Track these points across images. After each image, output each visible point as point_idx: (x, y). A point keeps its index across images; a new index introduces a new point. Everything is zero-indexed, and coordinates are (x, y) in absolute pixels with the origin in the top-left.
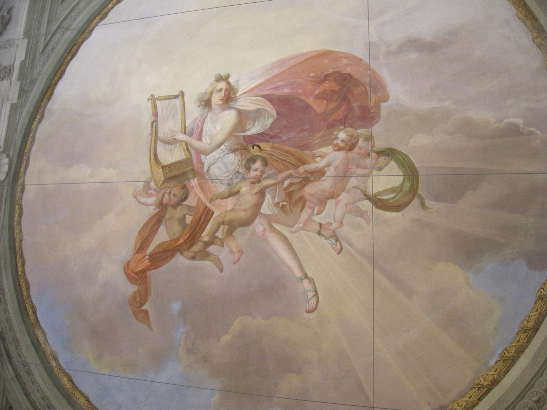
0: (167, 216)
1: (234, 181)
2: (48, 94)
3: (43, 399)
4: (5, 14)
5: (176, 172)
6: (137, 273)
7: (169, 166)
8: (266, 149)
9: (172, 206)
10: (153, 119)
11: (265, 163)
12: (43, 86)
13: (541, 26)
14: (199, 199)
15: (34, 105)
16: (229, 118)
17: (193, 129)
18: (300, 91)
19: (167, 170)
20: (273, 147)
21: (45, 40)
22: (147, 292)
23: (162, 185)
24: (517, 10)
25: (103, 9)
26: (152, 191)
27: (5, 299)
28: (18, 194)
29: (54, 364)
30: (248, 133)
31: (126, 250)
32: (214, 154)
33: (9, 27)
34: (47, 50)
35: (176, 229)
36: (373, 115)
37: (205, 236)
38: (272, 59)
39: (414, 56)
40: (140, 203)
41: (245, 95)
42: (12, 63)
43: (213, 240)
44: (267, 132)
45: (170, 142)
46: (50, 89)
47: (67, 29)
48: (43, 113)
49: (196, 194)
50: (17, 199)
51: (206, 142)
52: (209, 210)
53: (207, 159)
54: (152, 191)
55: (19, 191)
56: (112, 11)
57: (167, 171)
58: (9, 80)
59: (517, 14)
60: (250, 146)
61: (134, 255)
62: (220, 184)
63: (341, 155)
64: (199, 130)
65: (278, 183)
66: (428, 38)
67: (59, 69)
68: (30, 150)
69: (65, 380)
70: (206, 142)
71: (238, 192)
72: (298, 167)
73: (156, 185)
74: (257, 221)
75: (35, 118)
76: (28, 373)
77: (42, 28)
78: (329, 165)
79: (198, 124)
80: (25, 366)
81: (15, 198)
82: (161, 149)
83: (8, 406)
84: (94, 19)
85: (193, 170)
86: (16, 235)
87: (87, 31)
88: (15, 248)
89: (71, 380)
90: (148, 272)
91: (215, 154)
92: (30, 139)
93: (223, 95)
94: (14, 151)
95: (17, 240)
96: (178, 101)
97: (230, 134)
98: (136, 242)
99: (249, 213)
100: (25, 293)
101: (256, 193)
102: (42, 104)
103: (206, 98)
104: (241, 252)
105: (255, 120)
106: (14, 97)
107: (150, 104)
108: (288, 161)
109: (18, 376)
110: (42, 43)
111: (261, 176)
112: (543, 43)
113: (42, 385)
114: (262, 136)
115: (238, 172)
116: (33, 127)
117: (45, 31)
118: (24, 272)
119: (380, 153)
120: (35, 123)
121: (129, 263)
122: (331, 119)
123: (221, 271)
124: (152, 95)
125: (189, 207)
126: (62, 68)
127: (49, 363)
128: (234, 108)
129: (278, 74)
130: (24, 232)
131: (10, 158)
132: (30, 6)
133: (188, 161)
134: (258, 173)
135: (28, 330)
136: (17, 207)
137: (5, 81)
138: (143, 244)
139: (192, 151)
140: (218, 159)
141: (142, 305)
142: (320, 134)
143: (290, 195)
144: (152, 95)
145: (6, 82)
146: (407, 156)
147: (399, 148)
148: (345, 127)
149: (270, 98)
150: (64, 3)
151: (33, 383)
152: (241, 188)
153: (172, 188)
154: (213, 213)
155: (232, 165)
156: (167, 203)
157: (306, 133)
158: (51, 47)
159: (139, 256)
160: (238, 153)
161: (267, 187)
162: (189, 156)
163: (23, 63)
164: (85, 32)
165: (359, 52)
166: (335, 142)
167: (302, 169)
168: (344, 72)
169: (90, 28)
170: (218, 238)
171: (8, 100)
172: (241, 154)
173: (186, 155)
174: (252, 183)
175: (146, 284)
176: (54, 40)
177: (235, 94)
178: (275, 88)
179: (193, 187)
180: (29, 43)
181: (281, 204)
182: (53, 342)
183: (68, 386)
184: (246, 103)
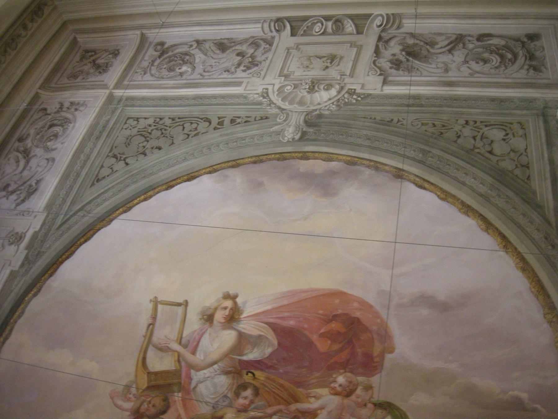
2: (52, 270)
4: (34, 184)
5: (161, 382)
7: (156, 373)
10: (150, 321)
11: (257, 392)
12: (48, 261)
13: (553, 303)
16: (228, 338)
18: (306, 326)
19: (153, 377)
20: (267, 378)
23: (144, 390)
24: (531, 284)
25: (128, 203)
26: (131, 396)
30: (245, 358)
32: (205, 371)
33: (32, 196)
34: (62, 228)
36: (375, 364)
38: (284, 288)
39: (424, 312)
40: (116, 405)
41: (250, 318)
42: (24, 231)
44: (265, 361)
45: (163, 349)
46: (55, 266)
51: (199, 357)
53: (196, 375)
54: (131, 396)
56: (137, 206)
58: (16, 247)
59: (530, 288)
60: (244, 372)
63: (336, 400)
64: (195, 344)
66: (441, 297)
68: (16, 322)
70: (199, 357)
72: (289, 404)
75: (31, 290)
78: (322, 408)
79: (195, 338)
82: (151, 354)
84: (117, 210)
85: (180, 383)
87: (107, 219)
91: (206, 373)
92: (19, 310)
93: (227, 314)
96: (180, 310)
97: (226, 355)
102: (43, 278)
103: (209, 312)
106: (16, 264)
107: (151, 306)
108: (281, 395)
110: (60, 220)
111: (249, 405)
112: (554, 320)
114: (258, 364)
116: (26, 299)
119: (378, 405)
120: (30, 295)
122: (332, 361)
126: (73, 249)
128: (235, 329)
132: (59, 183)
133: (176, 373)
134: (247, 402)
137: (13, 246)
139: (183, 364)
140: (208, 377)
142: (318, 374)
144: (156, 297)
145: (13, 248)
146: (405, 414)
147: (398, 404)
148: (345, 372)
149: (273, 327)
150: (93, 187)
152: (225, 414)
153: (153, 397)
157: (304, 370)
158: (68, 226)
160: (231, 376)
162: (179, 368)
163: (35, 235)
164: (106, 219)
165: (371, 298)
166: (332, 385)
167: (293, 407)
168: (353, 316)
169: (111, 217)
171: (10, 265)
172: (233, 377)
174: (239, 411)
176: (74, 220)
177: (239, 315)
180: (47, 216)
184: (248, 327)
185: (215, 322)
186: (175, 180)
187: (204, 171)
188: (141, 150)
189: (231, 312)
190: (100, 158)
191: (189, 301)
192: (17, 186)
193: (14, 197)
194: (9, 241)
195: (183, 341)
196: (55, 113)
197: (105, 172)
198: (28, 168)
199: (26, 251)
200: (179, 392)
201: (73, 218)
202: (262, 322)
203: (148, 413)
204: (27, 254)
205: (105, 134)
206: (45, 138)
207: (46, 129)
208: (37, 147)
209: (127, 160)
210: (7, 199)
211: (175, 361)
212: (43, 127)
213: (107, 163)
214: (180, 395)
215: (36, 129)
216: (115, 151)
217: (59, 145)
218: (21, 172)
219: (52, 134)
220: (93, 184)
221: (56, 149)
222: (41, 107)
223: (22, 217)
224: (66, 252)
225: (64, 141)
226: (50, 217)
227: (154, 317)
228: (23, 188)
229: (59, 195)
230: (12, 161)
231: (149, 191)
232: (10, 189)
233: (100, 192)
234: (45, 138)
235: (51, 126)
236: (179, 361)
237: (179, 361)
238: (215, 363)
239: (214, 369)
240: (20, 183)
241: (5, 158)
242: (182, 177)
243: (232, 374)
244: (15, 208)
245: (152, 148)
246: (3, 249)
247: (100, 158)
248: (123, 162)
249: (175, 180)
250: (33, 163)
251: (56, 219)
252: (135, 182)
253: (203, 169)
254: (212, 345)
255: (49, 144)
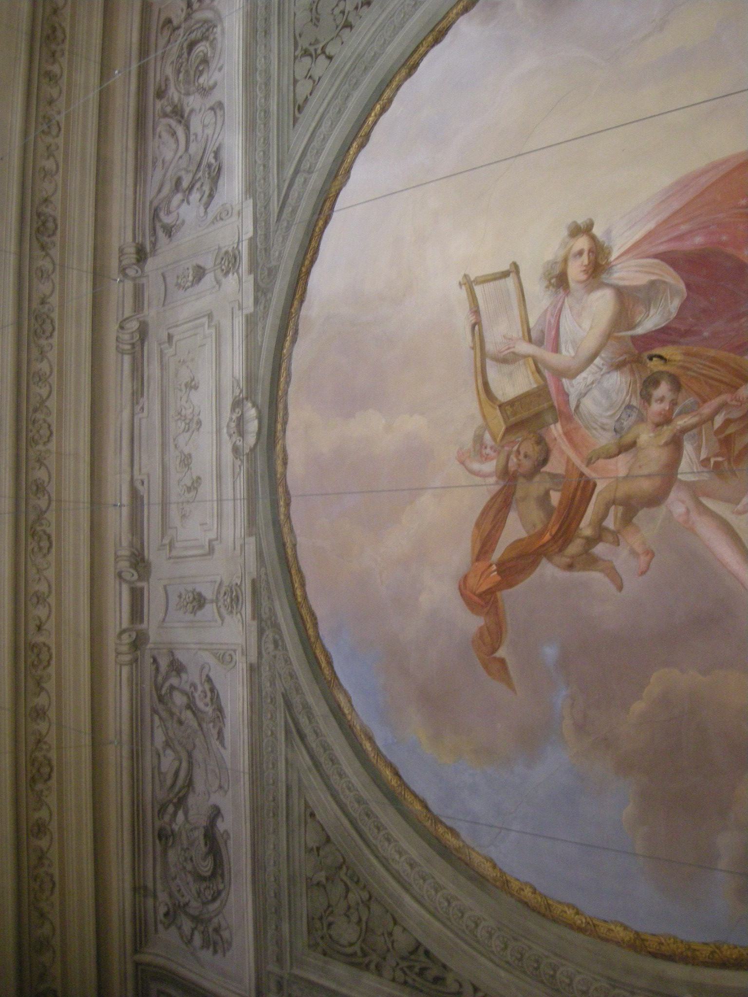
0: (519, 493)
1: (625, 423)
2: (299, 293)
3: (359, 802)
5: (525, 414)
6: (480, 596)
7: (512, 403)
8: (673, 357)
9: (524, 476)
10: (473, 319)
11: (676, 384)
12: (288, 278)
14: (568, 460)
15: (280, 313)
16: (600, 305)
17: (543, 332)
20: (687, 354)
21: (279, 195)
22: (501, 628)
23: (504, 435)
27: (283, 641)
28: (279, 469)
29: (368, 746)
30: (639, 331)
31: (458, 555)
33: (220, 182)
35: (536, 516)
37: (586, 526)
38: (665, 179)
40: (471, 472)
41: (624, 258)
43: (600, 534)
45: (508, 359)
46: (301, 282)
47: (310, 171)
48: (297, 325)
49: (562, 452)
50: (278, 476)
52: (588, 481)
54: (488, 451)
55: (279, 462)
56: (376, 128)
57: (509, 413)
61: (473, 564)
62: (600, 430)
64: (553, 333)
65: (704, 422)
67: (308, 248)
68: (286, 393)
69: (388, 773)
70: (567, 354)
71: (633, 444)
72: (736, 388)
73: (494, 439)
74: (673, 495)
75: (286, 336)
76: (332, 760)
77: (271, 175)
80: (325, 750)
81: (276, 475)
82: (493, 373)
83: (308, 813)
84: (349, 148)
86: (285, 536)
87: (342, 171)
88: (286, 558)
89: (397, 774)
90: (498, 594)
91: (586, 376)
92: (284, 373)
93: (586, 262)
94: (262, 397)
95: (289, 545)
96: (510, 283)
97: (609, 336)
98: (474, 542)
99: (657, 481)
100: (311, 632)
101: (667, 444)
102: (293, 310)
103: (557, 270)
104: (650, 553)
105: (648, 303)
107: (463, 293)
109: (317, 765)
110: (276, 203)
111: (671, 410)
113: (354, 780)
114: (664, 335)
115: (629, 407)
117: (276, 181)
118: (305, 597)
120: (287, 344)
121: (466, 577)
123: (620, 588)
124: (466, 276)
125: (553, 476)
126: (313, 243)
127: (361, 745)
129: (681, 209)
130: (297, 531)
131: (257, 407)
133: (541, 393)
134: (665, 406)
135: (323, 692)
136: (280, 490)
137: (230, 275)
138: (484, 546)
139: (546, 373)
140: (593, 383)
141: (495, 650)
143: (726, 442)
149: (670, 259)
151: (340, 775)
152: (638, 437)
154: (595, 485)
155: (617, 394)
156: (515, 472)
159: (482, 565)
160: (626, 369)
161: (684, 430)
162: (542, 383)
163: (252, 241)
169: (345, 165)
170: (606, 529)
172: (632, 372)
173: (536, 381)
174: (658, 425)
175: (497, 614)
176: (294, 194)
177: (607, 258)
178: (680, 238)
179: (555, 439)
180: (255, 206)
181: (712, 461)
182: (363, 711)
183: (394, 782)
184: (628, 273)
185: (572, 284)
186: (415, 51)
187: (455, 11)
188: (341, 21)
189: (592, 257)
190: (286, 68)
191: (518, 263)
192: (191, 175)
193: (195, 196)
194: (223, 270)
195: (534, 334)
196: (186, 20)
197: (304, 88)
198: (192, 137)
199: (252, 276)
200: (556, 421)
201: (291, 193)
202: (648, 257)
203: (521, 471)
204: (255, 280)
205: (274, 19)
206: (192, 73)
207: (185, 55)
208: (188, 94)
209: (327, 51)
210: (188, 203)
211: (533, 373)
212: (180, 57)
213: (300, 73)
214: (559, 425)
215: (173, 62)
216: (304, 43)
217: (216, 76)
218: (187, 149)
219: (198, 61)
220: (295, 120)
221: (215, 85)
222: (161, 23)
223: (221, 223)
224: (306, 254)
225: (221, 62)
226: (259, 205)
227: (476, 311)
228: (200, 174)
229: (255, 162)
230: (166, 136)
231: (384, 91)
232: (185, 184)
233: (311, 129)
234: (192, 73)
235: (192, 45)
236: (538, 371)
237: (538, 371)
238: (595, 355)
239: (598, 367)
240: (193, 168)
241: (154, 138)
242: (424, 39)
243: (628, 366)
244: (206, 212)
245: (356, 8)
246: (220, 286)
247: (286, 68)
248: (322, 57)
249: (415, 51)
250: (195, 125)
251: (268, 204)
252: (356, 84)
253: (452, 9)
254: (580, 327)
255: (201, 80)
